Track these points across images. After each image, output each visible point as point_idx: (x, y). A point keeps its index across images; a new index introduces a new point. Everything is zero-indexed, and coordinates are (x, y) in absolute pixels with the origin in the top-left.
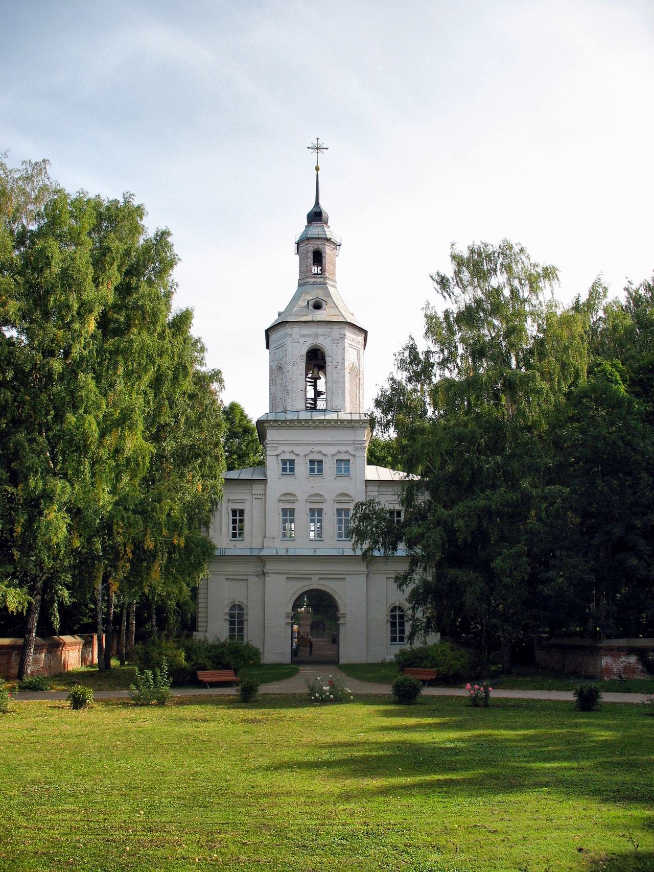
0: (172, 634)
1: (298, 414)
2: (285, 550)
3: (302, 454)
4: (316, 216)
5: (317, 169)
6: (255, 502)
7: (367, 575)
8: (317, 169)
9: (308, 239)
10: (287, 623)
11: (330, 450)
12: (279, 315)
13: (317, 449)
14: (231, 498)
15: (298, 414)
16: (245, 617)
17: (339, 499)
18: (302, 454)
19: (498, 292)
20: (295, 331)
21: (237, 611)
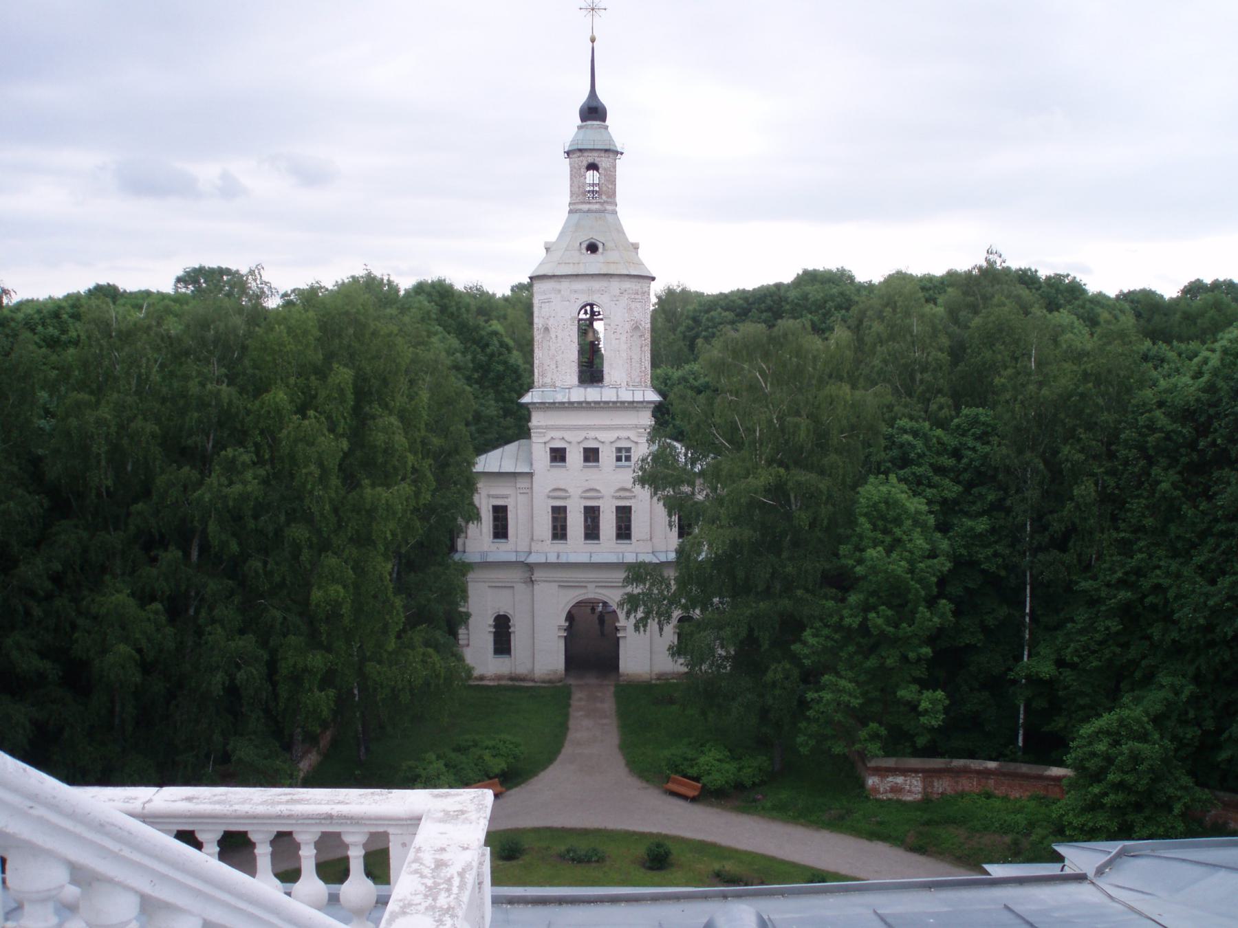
1: (569, 392)
2: (556, 554)
4: (593, 112)
5: (593, 40)
6: (521, 498)
8: (593, 40)
10: (559, 637)
11: (606, 436)
12: (547, 249)
13: (592, 434)
14: (492, 492)
15: (569, 392)
17: (618, 494)
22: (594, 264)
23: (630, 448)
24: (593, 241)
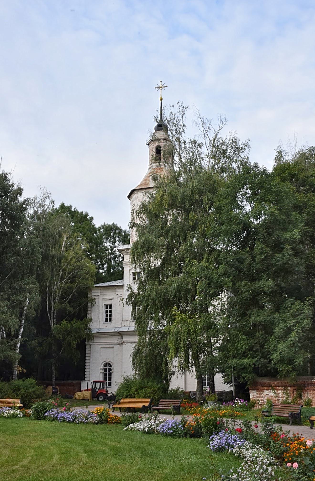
0: (26, 305)
5: (161, 100)
16: (112, 371)
19: (112, 231)
21: (108, 367)
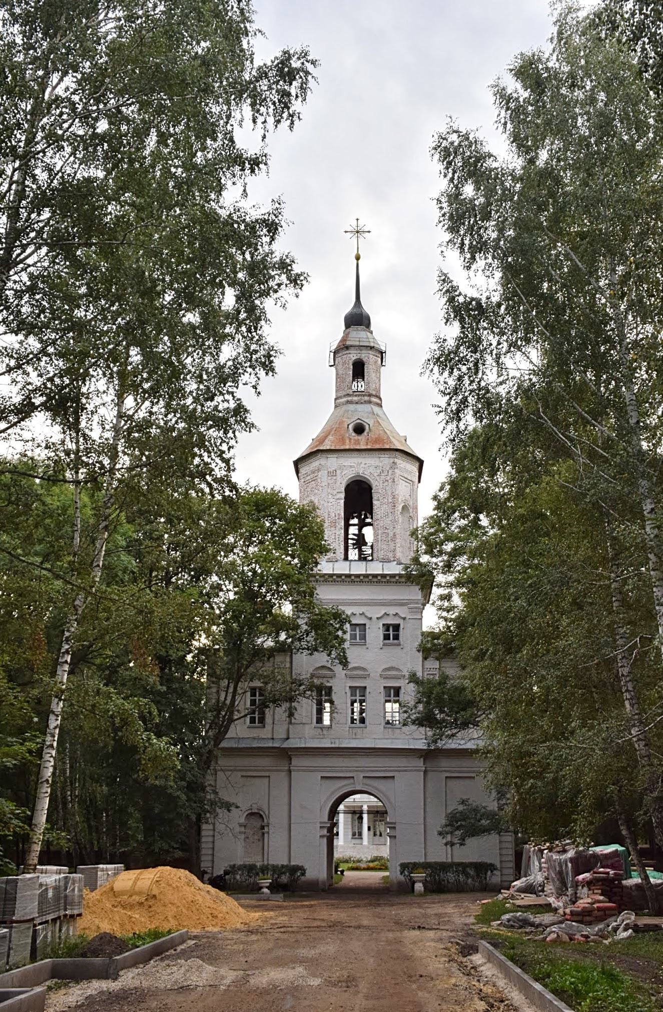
3: (374, 617)
5: (358, 258)
7: (425, 772)
8: (358, 258)
9: (347, 348)
18: (374, 617)
20: (332, 462)
22: (362, 442)
23: (399, 625)
24: (359, 421)
